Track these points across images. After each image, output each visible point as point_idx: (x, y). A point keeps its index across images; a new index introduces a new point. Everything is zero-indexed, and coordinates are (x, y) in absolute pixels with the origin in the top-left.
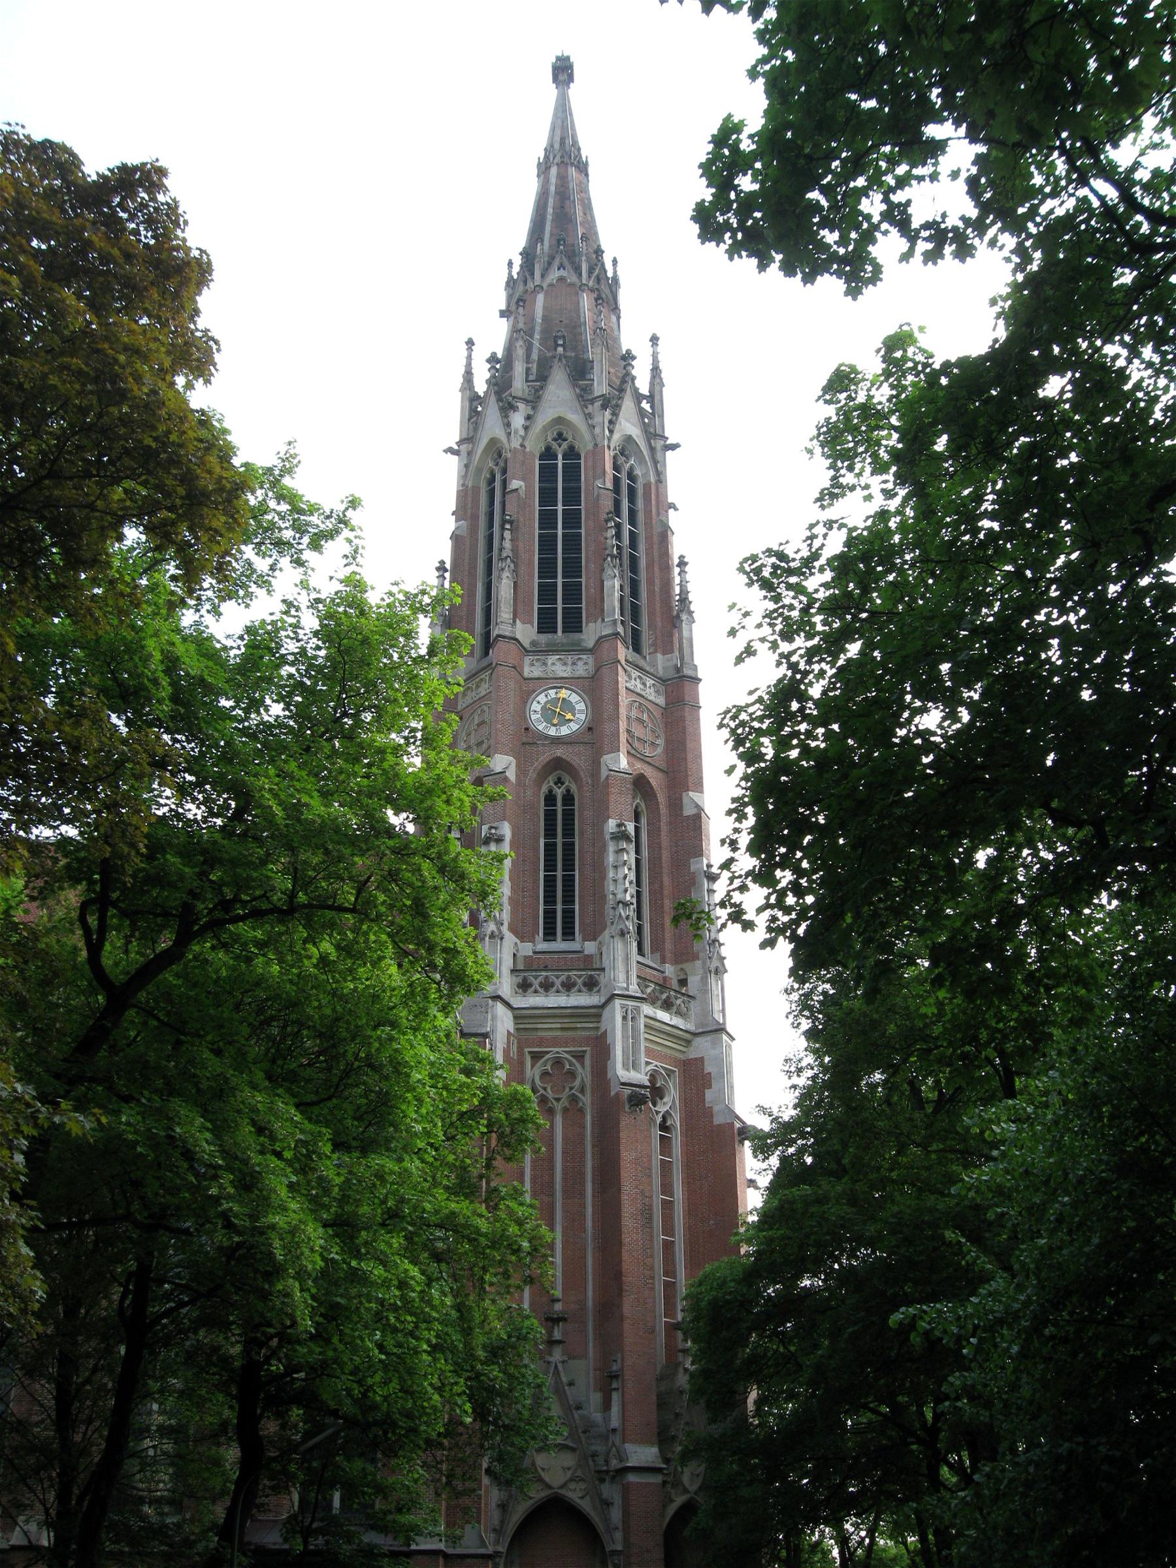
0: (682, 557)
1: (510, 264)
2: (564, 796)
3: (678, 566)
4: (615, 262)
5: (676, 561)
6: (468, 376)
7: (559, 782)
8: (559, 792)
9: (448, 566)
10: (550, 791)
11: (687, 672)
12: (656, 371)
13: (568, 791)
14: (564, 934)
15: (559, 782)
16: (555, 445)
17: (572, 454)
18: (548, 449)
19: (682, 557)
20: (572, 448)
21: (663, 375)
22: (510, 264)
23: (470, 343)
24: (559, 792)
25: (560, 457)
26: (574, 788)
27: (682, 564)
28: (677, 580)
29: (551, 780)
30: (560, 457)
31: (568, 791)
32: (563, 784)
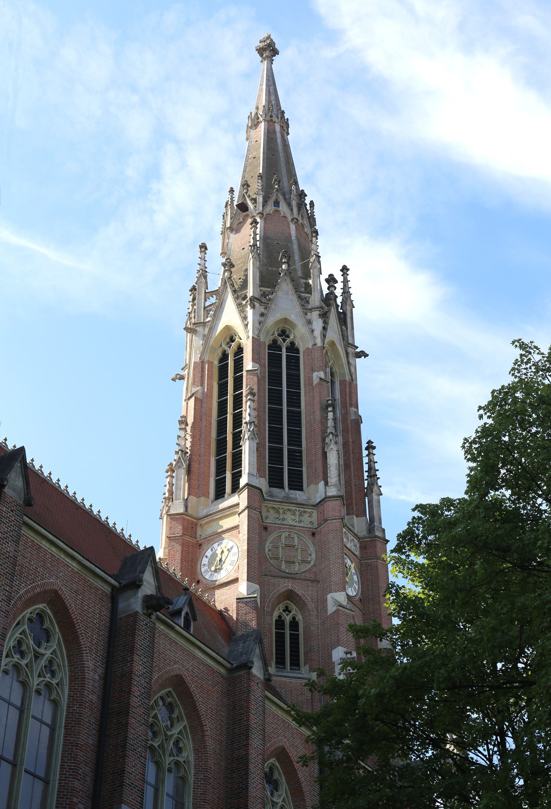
0: (369, 442)
1: (232, 191)
2: (290, 622)
3: (367, 449)
4: (161, 518)
5: (364, 445)
6: (203, 274)
7: (287, 610)
8: (288, 619)
9: (255, 391)
10: (280, 617)
11: (378, 533)
12: (346, 293)
13: (294, 618)
14: (277, 663)
15: (287, 610)
16: (280, 339)
17: (293, 349)
18: (275, 341)
19: (369, 442)
20: (293, 344)
21: (352, 298)
22: (232, 191)
23: (203, 247)
24: (288, 619)
25: (284, 350)
26: (299, 617)
27: (370, 446)
28: (365, 460)
29: (281, 606)
30: (284, 350)
31: (294, 618)
32: (290, 612)
